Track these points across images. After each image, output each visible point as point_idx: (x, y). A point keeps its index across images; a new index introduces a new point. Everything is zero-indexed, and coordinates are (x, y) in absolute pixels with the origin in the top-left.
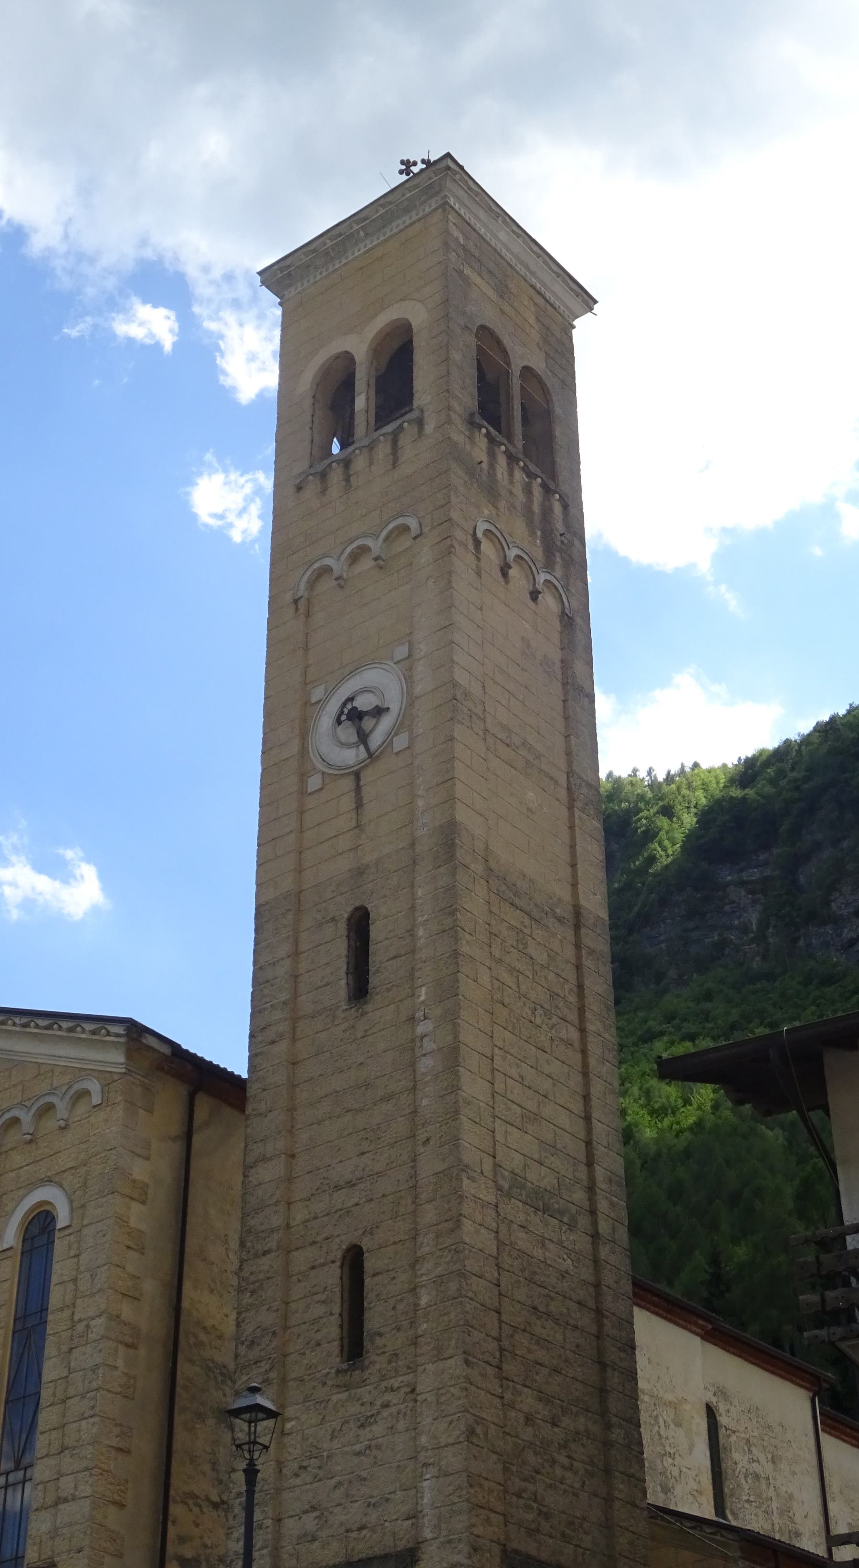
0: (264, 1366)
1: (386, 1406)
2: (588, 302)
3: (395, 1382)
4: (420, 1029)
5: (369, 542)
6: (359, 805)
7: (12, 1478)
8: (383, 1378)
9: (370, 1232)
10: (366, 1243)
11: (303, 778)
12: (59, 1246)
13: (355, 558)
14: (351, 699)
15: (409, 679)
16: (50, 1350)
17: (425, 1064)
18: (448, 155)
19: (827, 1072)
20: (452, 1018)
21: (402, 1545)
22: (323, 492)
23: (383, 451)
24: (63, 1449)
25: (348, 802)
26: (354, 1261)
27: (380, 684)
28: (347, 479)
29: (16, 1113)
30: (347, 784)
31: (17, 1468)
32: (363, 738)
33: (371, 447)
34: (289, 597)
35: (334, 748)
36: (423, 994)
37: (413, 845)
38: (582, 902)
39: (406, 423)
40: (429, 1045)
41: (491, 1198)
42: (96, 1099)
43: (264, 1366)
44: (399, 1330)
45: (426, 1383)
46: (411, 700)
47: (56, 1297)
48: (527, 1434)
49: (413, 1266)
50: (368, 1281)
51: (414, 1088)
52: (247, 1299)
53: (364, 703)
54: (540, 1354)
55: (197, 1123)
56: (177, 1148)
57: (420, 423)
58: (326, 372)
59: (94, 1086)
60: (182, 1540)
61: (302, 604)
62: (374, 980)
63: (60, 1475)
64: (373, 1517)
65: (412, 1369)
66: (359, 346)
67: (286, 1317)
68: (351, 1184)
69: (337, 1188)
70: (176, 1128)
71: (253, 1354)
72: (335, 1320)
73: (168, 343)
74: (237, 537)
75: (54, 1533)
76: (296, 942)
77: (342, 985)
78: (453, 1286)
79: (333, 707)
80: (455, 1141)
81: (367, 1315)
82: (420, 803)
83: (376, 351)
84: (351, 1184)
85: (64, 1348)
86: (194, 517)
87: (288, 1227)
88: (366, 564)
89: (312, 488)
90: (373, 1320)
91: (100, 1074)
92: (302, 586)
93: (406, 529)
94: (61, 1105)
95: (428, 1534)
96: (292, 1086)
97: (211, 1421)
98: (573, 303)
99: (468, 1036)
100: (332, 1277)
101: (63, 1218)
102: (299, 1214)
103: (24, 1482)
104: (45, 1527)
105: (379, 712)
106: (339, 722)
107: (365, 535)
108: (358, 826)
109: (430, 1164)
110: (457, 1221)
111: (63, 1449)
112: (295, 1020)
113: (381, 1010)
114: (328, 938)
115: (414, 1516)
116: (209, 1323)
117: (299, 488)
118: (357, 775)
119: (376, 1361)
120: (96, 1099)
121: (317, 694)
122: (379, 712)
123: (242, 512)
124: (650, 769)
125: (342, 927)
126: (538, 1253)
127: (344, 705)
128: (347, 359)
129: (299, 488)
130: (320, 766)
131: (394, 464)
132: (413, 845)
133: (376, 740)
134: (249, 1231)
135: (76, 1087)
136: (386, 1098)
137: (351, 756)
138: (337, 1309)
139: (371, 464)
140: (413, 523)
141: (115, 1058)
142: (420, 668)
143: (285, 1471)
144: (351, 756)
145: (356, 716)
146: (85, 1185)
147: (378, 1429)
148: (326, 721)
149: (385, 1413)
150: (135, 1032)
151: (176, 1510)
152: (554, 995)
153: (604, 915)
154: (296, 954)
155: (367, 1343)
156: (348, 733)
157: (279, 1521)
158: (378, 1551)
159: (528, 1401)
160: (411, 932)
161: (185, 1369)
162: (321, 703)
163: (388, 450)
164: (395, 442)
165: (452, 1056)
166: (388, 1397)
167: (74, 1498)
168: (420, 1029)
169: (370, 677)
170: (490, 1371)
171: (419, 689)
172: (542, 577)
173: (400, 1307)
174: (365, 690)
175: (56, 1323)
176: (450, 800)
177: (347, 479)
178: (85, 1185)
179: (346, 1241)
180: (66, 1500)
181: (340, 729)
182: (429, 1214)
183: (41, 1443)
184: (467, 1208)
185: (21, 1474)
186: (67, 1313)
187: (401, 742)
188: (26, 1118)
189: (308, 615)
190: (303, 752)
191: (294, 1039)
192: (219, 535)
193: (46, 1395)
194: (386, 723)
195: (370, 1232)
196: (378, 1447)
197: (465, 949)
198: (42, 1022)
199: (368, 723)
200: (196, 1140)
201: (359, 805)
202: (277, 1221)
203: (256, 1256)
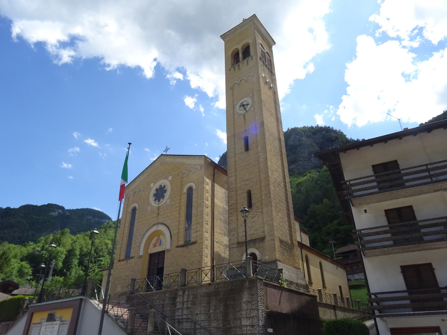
0: (234, 209)
4: (259, 154)
5: (244, 78)
6: (245, 120)
9: (252, 187)
10: (251, 189)
11: (234, 116)
13: (241, 81)
15: (253, 99)
16: (193, 208)
19: (340, 157)
21: (261, 237)
22: (235, 70)
25: (243, 119)
26: (249, 194)
28: (239, 68)
30: (243, 117)
32: (245, 109)
36: (259, 149)
39: (250, 59)
40: (261, 157)
43: (234, 209)
52: (229, 199)
53: (245, 103)
56: (213, 177)
57: (252, 58)
59: (199, 167)
62: (250, 147)
70: (212, 174)
71: (231, 208)
72: (246, 201)
75: (197, 237)
79: (239, 104)
83: (242, 48)
88: (243, 81)
90: (253, 202)
93: (251, 75)
95: (266, 234)
96: (235, 165)
100: (245, 195)
101: (194, 187)
105: (247, 105)
109: (263, 176)
112: (235, 155)
113: (251, 152)
119: (254, 207)
121: (236, 103)
122: (247, 105)
124: (403, 75)
133: (247, 109)
140: (252, 74)
141: (202, 162)
144: (243, 112)
145: (243, 105)
148: (238, 107)
154: (235, 144)
156: (242, 108)
157: (238, 234)
158: (257, 238)
160: (257, 139)
162: (237, 104)
164: (247, 61)
165: (266, 159)
166: (257, 213)
168: (259, 154)
169: (245, 99)
174: (244, 101)
175: (194, 204)
177: (239, 68)
182: (263, 184)
183: (193, 223)
190: (234, 112)
194: (249, 106)
195: (252, 187)
199: (246, 106)
201: (245, 120)
202: (234, 186)
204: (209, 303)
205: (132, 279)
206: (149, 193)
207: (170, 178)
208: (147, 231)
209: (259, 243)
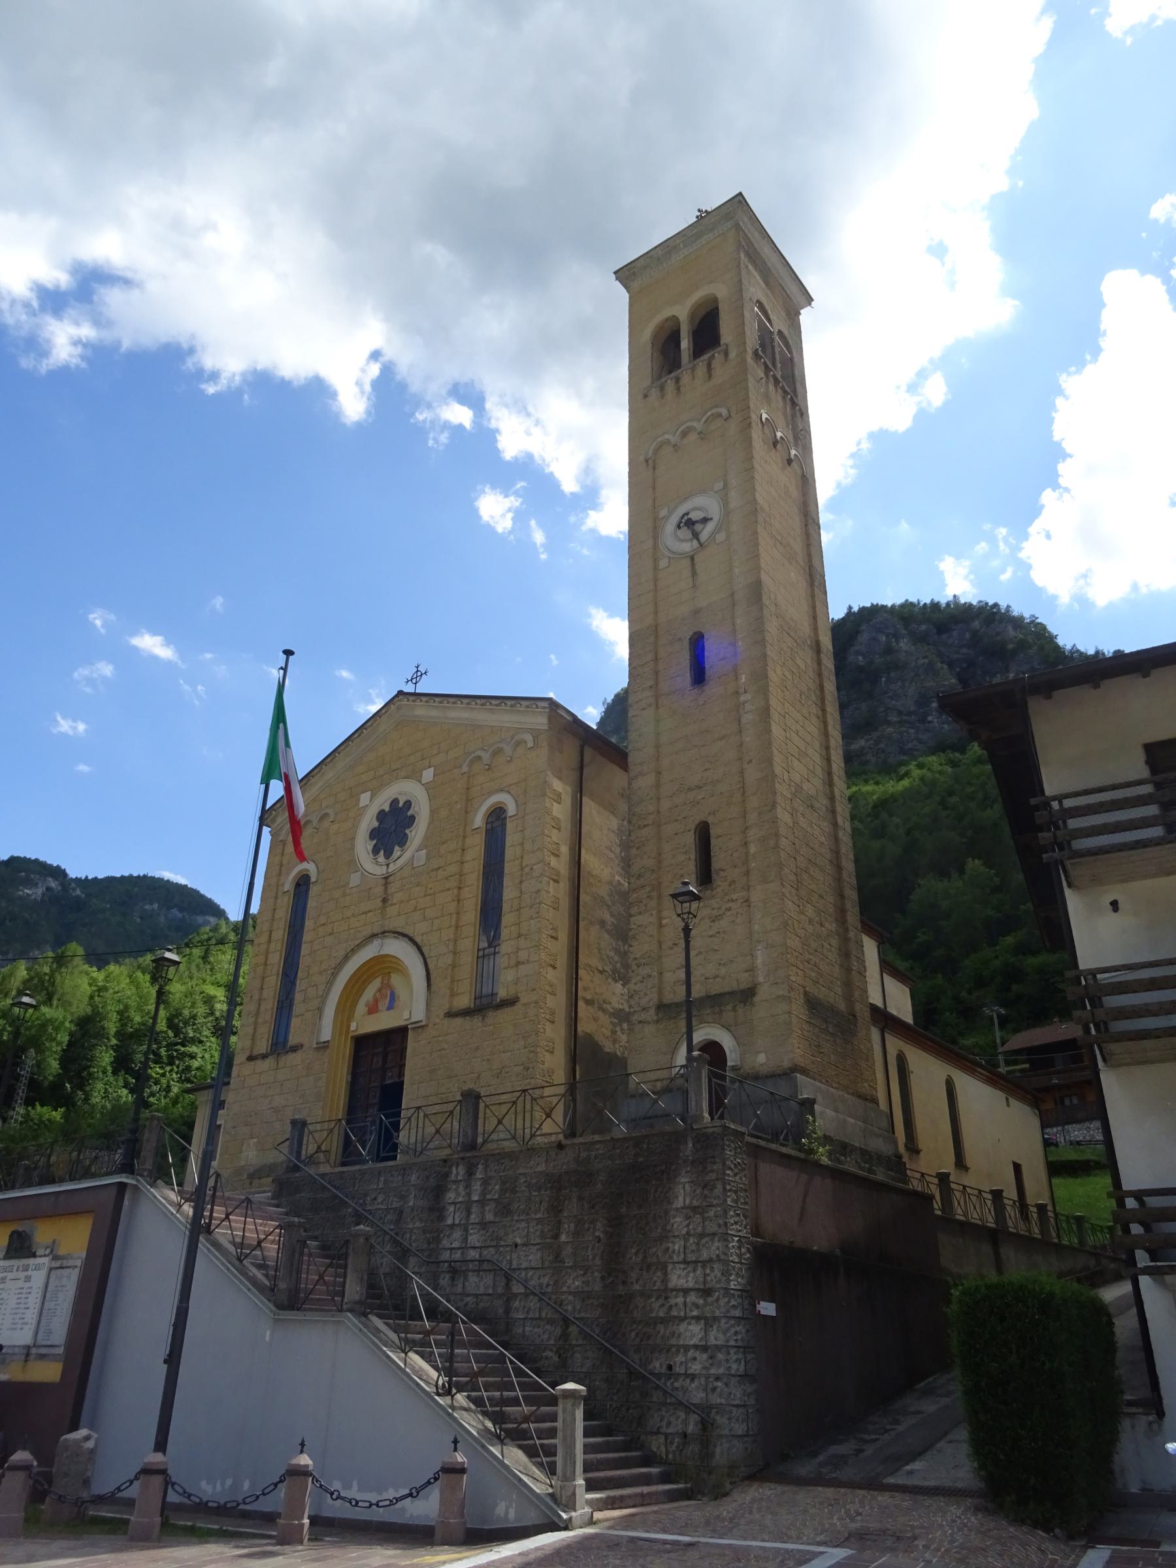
0: (648, 889)
1: (729, 909)
2: (809, 300)
3: (734, 897)
4: (742, 698)
5: (695, 424)
6: (694, 573)
7: (487, 951)
8: (726, 894)
10: (710, 820)
12: (510, 826)
13: (684, 434)
14: (687, 514)
15: (725, 502)
16: (507, 881)
17: (747, 718)
18: (740, 194)
20: (764, 691)
22: (663, 396)
23: (701, 369)
24: (520, 936)
25: (687, 573)
27: (706, 504)
28: (678, 389)
29: (480, 753)
30: (687, 562)
31: (490, 946)
32: (696, 535)
33: (693, 369)
34: (642, 458)
35: (675, 542)
36: (743, 679)
37: (732, 595)
38: (821, 638)
40: (748, 707)
41: (789, 796)
42: (530, 744)
43: (648, 889)
44: (735, 867)
45: (756, 896)
46: (727, 512)
47: (509, 853)
48: (810, 929)
49: (744, 832)
50: (713, 841)
51: (740, 732)
53: (694, 516)
54: (813, 887)
55: (586, 761)
57: (726, 354)
58: (660, 328)
59: (529, 738)
60: (585, 989)
61: (650, 462)
63: (519, 949)
64: (723, 971)
65: (748, 888)
66: (682, 312)
67: (659, 862)
68: (699, 787)
69: (690, 789)
73: (468, 424)
74: (500, 530)
75: (516, 982)
76: (656, 653)
77: (688, 677)
78: (772, 843)
79: (674, 519)
80: (769, 761)
81: (713, 859)
82: (736, 571)
83: (692, 316)
84: (699, 787)
85: (517, 881)
86: (479, 517)
87: (658, 812)
88: (693, 437)
89: (654, 393)
91: (531, 731)
92: (651, 452)
93: (720, 415)
94: (508, 750)
95: (761, 979)
97: (597, 927)
98: (800, 298)
99: (773, 702)
100: (690, 839)
101: (511, 809)
102: (665, 805)
103: (495, 954)
104: (510, 978)
105: (705, 520)
106: (679, 527)
107: (691, 420)
108: (694, 586)
109: (753, 774)
110: (774, 805)
111: (520, 936)
112: (657, 697)
113: (713, 688)
114: (677, 650)
115: (752, 970)
116: (594, 873)
117: (645, 396)
118: (692, 558)
120: (530, 744)
122: (705, 520)
123: (503, 516)
125: (686, 643)
126: (809, 829)
127: (683, 517)
128: (674, 320)
129: (645, 396)
130: (667, 553)
131: (710, 377)
132: (732, 595)
133: (704, 536)
134: (634, 815)
135: (517, 738)
136: (721, 739)
137: (687, 547)
138: (693, 857)
139: (693, 379)
140: (724, 412)
141: (541, 721)
142: (732, 493)
143: (664, 946)
144: (687, 547)
145: (690, 523)
146: (525, 792)
147: (724, 923)
149: (729, 913)
150: (553, 705)
151: (581, 972)
152: (809, 689)
153: (830, 647)
154: (656, 660)
155: (714, 876)
156: (685, 533)
158: (727, 989)
159: (810, 911)
160: (734, 644)
161: (583, 897)
162: (666, 518)
163: (705, 370)
164: (709, 365)
167: (528, 961)
168: (742, 698)
169: (699, 501)
170: (794, 891)
171: (732, 505)
172: (793, 452)
173: (735, 855)
175: (510, 868)
176: (758, 568)
177: (678, 389)
178: (525, 792)
179: (698, 818)
180: (523, 963)
181: (679, 532)
183: (505, 933)
184: (779, 799)
185: (492, 950)
186: (517, 862)
187: (721, 537)
188: (486, 756)
189: (654, 468)
190: (655, 546)
191: (657, 708)
192: (489, 529)
193: (506, 907)
194: (710, 526)
196: (724, 932)
197: (769, 653)
198: (494, 702)
199: (698, 527)
200: (585, 772)
201: (694, 573)
202: (651, 808)
203: (639, 827)
204: (556, 1209)
205: (294, 1123)
206: (355, 826)
207: (428, 775)
208: (346, 958)
209: (734, 1009)
